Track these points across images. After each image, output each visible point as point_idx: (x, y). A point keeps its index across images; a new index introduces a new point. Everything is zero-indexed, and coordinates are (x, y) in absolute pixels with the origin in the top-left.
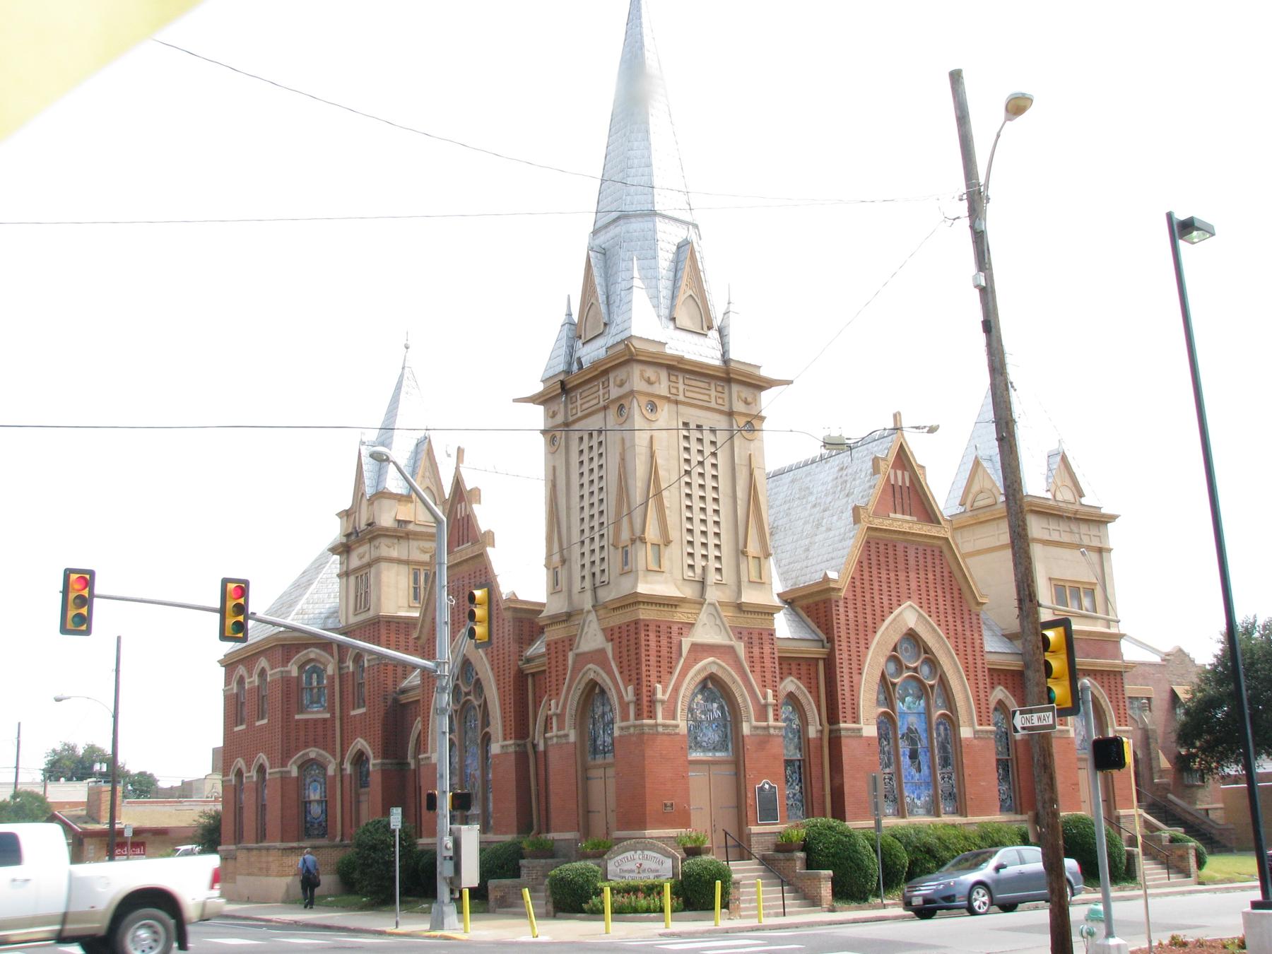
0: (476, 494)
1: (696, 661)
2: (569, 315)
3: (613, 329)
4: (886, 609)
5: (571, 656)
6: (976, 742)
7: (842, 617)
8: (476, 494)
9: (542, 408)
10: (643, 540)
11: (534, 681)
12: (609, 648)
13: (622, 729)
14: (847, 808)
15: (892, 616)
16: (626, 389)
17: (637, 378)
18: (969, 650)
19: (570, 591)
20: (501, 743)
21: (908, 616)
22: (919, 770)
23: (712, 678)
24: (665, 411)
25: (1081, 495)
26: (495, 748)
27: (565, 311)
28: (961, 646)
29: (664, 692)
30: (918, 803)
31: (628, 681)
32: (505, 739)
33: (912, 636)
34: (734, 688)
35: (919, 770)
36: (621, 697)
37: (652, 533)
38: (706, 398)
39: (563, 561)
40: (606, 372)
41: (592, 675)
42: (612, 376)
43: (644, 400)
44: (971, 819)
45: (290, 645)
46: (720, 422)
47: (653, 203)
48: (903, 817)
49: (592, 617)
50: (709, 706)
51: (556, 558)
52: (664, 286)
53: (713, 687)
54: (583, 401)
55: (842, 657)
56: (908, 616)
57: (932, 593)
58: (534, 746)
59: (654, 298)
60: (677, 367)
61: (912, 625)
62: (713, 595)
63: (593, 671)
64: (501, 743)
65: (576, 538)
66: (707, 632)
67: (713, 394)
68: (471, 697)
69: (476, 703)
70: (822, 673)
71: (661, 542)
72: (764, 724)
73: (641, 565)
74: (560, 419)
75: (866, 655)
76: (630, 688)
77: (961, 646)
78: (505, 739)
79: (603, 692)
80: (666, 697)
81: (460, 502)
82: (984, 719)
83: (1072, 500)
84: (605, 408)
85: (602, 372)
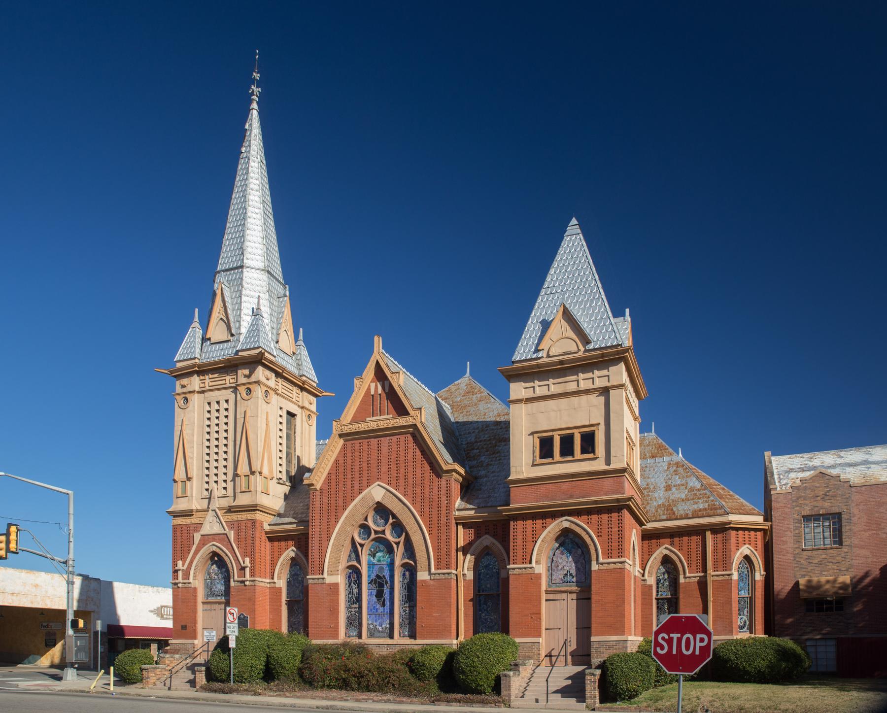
1: (204, 545)
4: (357, 491)
6: (432, 583)
7: (318, 504)
12: (232, 535)
14: (511, 629)
15: (361, 496)
17: (261, 373)
18: (435, 512)
21: (377, 492)
22: (384, 605)
23: (215, 554)
24: (195, 399)
28: (427, 509)
29: (183, 565)
30: (380, 629)
31: (244, 555)
33: (381, 510)
34: (226, 558)
35: (384, 605)
37: (180, 474)
38: (223, 382)
44: (419, 641)
46: (229, 394)
48: (415, 639)
53: (217, 559)
55: (314, 533)
56: (70, 492)
57: (402, 471)
66: (211, 526)
67: (229, 380)
70: (299, 543)
71: (249, 473)
72: (321, 576)
76: (247, 560)
77: (427, 509)
78: (438, 567)
82: (443, 563)
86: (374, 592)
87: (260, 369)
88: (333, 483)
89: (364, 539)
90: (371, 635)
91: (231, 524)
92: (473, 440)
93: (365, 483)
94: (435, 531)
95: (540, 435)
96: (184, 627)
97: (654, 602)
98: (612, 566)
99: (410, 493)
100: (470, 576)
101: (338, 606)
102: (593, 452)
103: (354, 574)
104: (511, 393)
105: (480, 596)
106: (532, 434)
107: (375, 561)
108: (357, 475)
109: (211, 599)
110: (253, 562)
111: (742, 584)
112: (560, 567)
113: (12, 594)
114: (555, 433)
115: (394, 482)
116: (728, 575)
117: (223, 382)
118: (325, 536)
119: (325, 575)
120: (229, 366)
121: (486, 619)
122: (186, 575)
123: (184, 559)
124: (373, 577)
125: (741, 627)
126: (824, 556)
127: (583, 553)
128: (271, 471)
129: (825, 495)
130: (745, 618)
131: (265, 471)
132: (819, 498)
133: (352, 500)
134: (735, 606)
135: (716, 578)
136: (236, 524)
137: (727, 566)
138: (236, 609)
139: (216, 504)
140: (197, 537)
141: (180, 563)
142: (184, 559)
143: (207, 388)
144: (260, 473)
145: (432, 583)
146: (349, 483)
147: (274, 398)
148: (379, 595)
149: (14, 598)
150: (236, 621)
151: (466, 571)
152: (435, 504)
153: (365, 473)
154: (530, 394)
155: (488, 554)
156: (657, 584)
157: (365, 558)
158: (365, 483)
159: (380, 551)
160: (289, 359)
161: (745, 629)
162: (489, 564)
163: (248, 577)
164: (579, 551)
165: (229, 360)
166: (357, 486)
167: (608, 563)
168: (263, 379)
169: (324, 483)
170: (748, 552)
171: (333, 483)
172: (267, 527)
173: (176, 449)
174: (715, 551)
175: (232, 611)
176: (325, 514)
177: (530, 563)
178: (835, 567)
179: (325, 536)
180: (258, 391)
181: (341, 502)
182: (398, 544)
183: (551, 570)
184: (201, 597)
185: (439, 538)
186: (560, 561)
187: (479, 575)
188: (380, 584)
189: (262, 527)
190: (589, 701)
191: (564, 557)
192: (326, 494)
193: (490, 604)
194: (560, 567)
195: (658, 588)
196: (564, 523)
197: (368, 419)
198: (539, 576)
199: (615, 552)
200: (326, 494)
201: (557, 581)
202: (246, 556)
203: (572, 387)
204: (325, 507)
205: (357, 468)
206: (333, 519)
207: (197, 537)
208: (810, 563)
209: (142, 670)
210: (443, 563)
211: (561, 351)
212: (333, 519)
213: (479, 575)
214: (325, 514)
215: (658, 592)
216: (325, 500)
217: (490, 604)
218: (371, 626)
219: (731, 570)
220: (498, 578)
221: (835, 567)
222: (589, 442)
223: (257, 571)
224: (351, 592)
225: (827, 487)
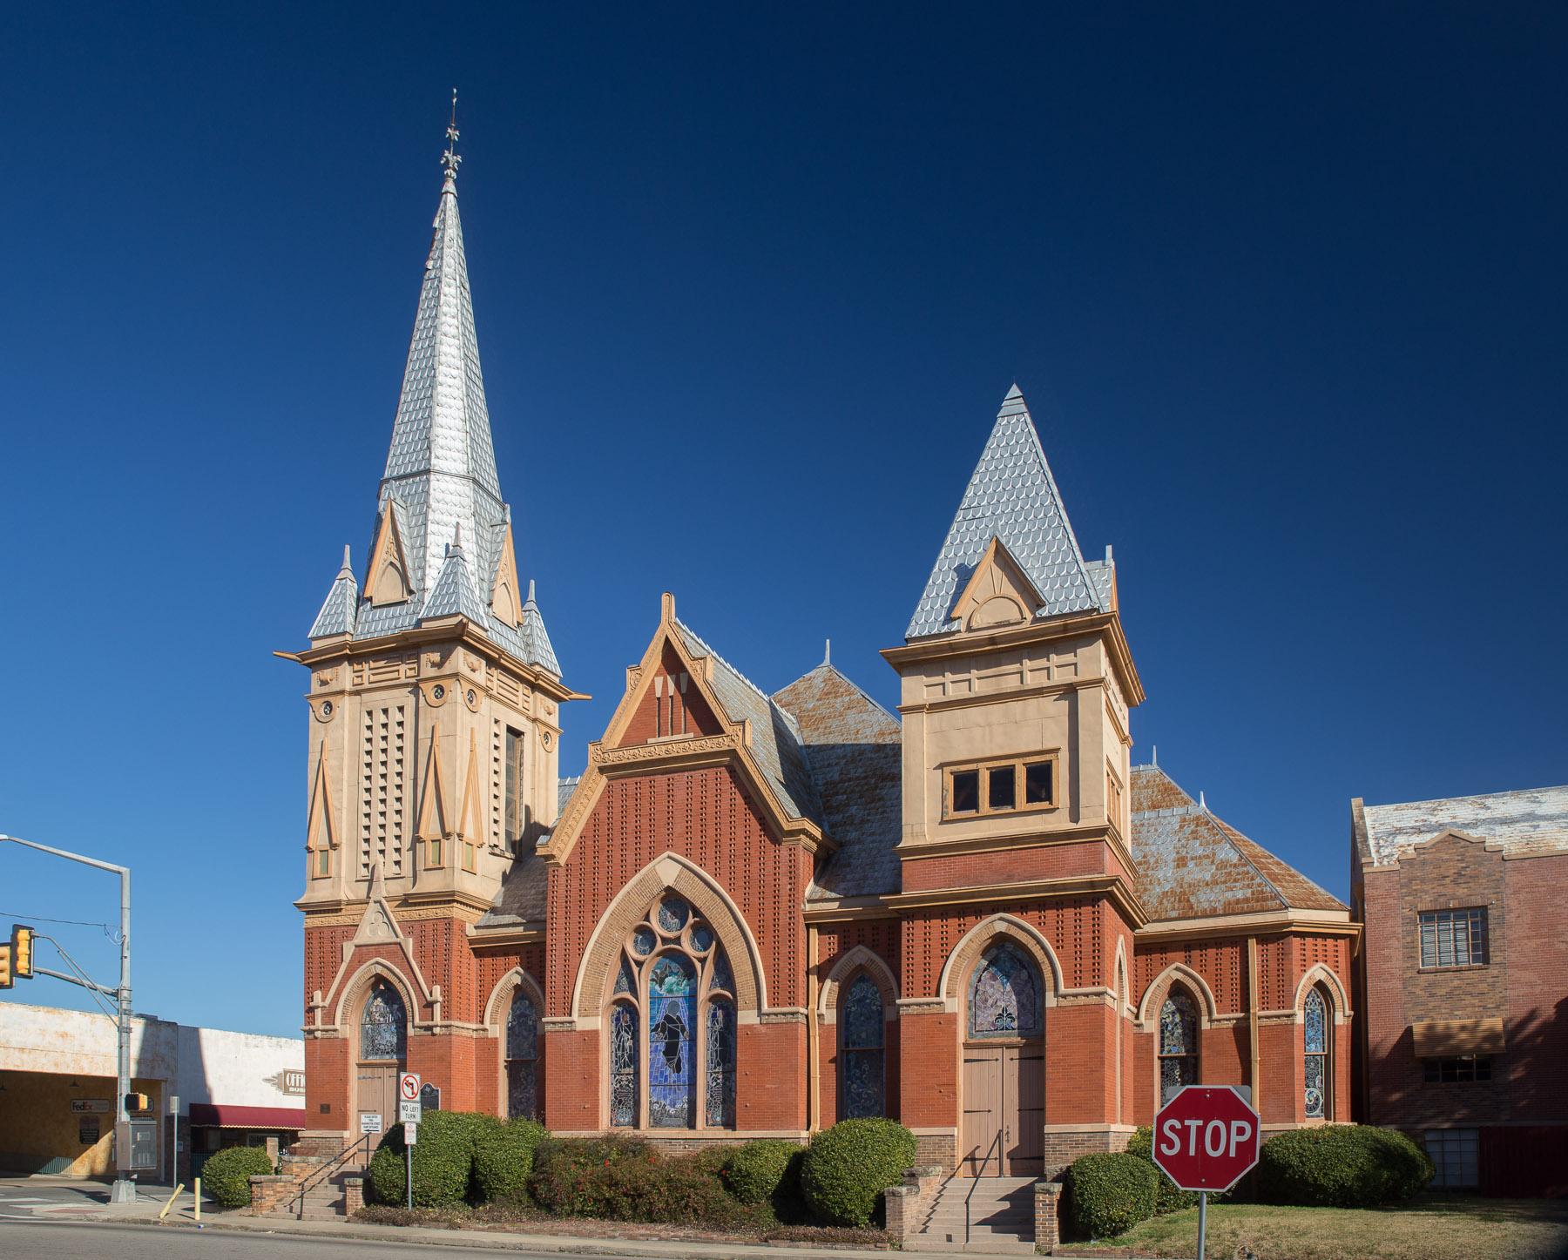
1: (361, 963)
6: (763, 1029)
12: (410, 946)
15: (638, 877)
16: (447, 669)
18: (769, 903)
21: (667, 870)
23: (379, 979)
25: (1036, 602)
28: (754, 900)
29: (323, 1000)
30: (672, 1111)
31: (432, 981)
33: (674, 901)
37: (318, 838)
38: (395, 675)
44: (740, 1133)
45: (456, 1121)
46: (404, 697)
50: (1426, 1022)
53: (383, 988)
55: (556, 941)
56: (123, 869)
57: (711, 832)
60: (1122, 849)
61: (669, 881)
62: (383, 890)
66: (373, 930)
67: (404, 671)
76: (437, 989)
80: (327, 1003)
82: (784, 995)
83: (1016, 616)
86: (662, 1046)
87: (460, 652)
88: (589, 853)
89: (644, 952)
90: (656, 1122)
91: (409, 927)
92: (836, 777)
93: (645, 854)
94: (769, 940)
95: (954, 768)
96: (325, 1109)
97: (1157, 1063)
99: (725, 871)
100: (831, 1017)
101: (597, 1071)
102: (1049, 798)
103: (626, 1014)
105: (848, 1053)
106: (941, 766)
107: (663, 992)
108: (631, 839)
109: (372, 1059)
110: (446, 993)
111: (1311, 1033)
112: (990, 1001)
114: (981, 765)
115: (696, 852)
116: (1288, 1016)
117: (395, 675)
118: (574, 947)
119: (575, 1016)
120: (406, 647)
121: (859, 1095)
122: (330, 1016)
123: (325, 989)
124: (660, 1019)
125: (1311, 1109)
126: (1456, 983)
128: (479, 832)
129: (1459, 874)
130: (1317, 1092)
131: (469, 833)
132: (1447, 881)
133: (623, 883)
134: (1299, 1071)
135: (1265, 1022)
136: (417, 925)
137: (1285, 999)
139: (383, 890)
140: (349, 949)
141: (318, 995)
142: (325, 989)
143: (366, 685)
144: (460, 836)
146: (617, 855)
147: (484, 703)
148: (671, 1051)
149: (25, 1056)
150: (418, 1098)
151: (823, 1010)
152: (769, 891)
153: (645, 836)
154: (936, 696)
155: (862, 980)
156: (1162, 1032)
157: (645, 986)
158: (645, 854)
159: (672, 973)
160: (510, 635)
161: (1318, 1111)
162: (865, 998)
163: (438, 1019)
164: (1024, 975)
165: (404, 637)
166: (631, 859)
167: (1075, 996)
168: (465, 670)
169: (573, 854)
170: (1321, 976)
171: (589, 853)
172: (471, 932)
173: (310, 793)
174: (1264, 973)
175: (411, 1080)
176: (574, 909)
177: (938, 995)
178: (1476, 1002)
179: (574, 947)
180: (457, 692)
181: (602, 887)
182: (703, 961)
183: (973, 1006)
184: (354, 1055)
185: (776, 951)
186: (990, 991)
187: (848, 1015)
188: (672, 1033)
189: (463, 931)
190: (1040, 1238)
191: (997, 984)
192: (576, 873)
193: (866, 1067)
194: (990, 1001)
195: (1162, 1039)
196: (997, 924)
197: (650, 741)
198: (952, 1018)
199: (1087, 976)
200: (576, 873)
202: (435, 982)
203: (1011, 684)
204: (574, 894)
205: (631, 827)
206: (589, 917)
207: (349, 949)
208: (1432, 995)
209: (250, 1184)
210: (784, 995)
211: (992, 621)
212: (589, 917)
213: (848, 1015)
214: (574, 909)
215: (1162, 1046)
216: (575, 883)
217: (866, 1067)
218: (656, 1107)
219: (1292, 1007)
220: (881, 1022)
221: (1476, 1002)
222: (1040, 780)
223: (454, 1010)
224: (621, 1047)
225: (1462, 861)
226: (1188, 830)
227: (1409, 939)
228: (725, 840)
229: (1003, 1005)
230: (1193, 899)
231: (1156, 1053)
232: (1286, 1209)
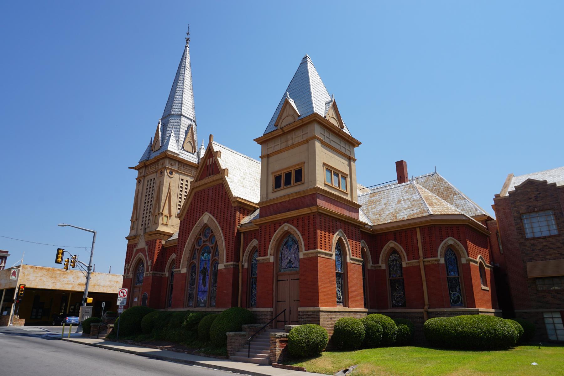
0: (218, 153)
2: (151, 143)
3: (163, 148)
5: (135, 250)
8: (218, 153)
9: (137, 171)
10: (162, 214)
11: (244, 236)
13: (304, 254)
19: (137, 229)
20: (225, 263)
22: (205, 286)
26: (221, 267)
27: (150, 142)
30: (202, 301)
32: (227, 262)
35: (205, 286)
36: (147, 263)
37: (166, 212)
39: (137, 219)
40: (158, 160)
41: (140, 256)
42: (160, 162)
43: (168, 171)
47: (181, 111)
49: (143, 237)
51: (135, 218)
52: (182, 136)
54: (150, 170)
58: (243, 266)
59: (177, 141)
63: (141, 255)
64: (225, 263)
65: (142, 212)
68: (208, 243)
69: (210, 246)
73: (160, 222)
74: (143, 174)
75: (332, 238)
76: (150, 261)
78: (227, 262)
79: (142, 262)
81: (209, 158)
84: (157, 172)
85: (157, 161)
98: (310, 256)
100: (246, 265)
104: (169, 146)
111: (450, 267)
113: (104, 286)
126: (544, 244)
127: (298, 247)
129: (537, 197)
132: (531, 200)
138: (127, 290)
145: (224, 271)
149: (104, 288)
154: (283, 146)
167: (308, 254)
173: (162, 204)
174: (423, 243)
178: (556, 252)
186: (286, 253)
191: (288, 250)
195: (390, 271)
196: (286, 227)
201: (284, 267)
205: (199, 205)
208: (534, 250)
215: (390, 274)
216: (185, 225)
219: (437, 256)
221: (556, 252)
222: (299, 174)
225: (537, 191)
226: (406, 190)
227: (518, 226)
228: (220, 207)
229: (289, 258)
230: (398, 215)
231: (387, 277)
232: (484, 352)
